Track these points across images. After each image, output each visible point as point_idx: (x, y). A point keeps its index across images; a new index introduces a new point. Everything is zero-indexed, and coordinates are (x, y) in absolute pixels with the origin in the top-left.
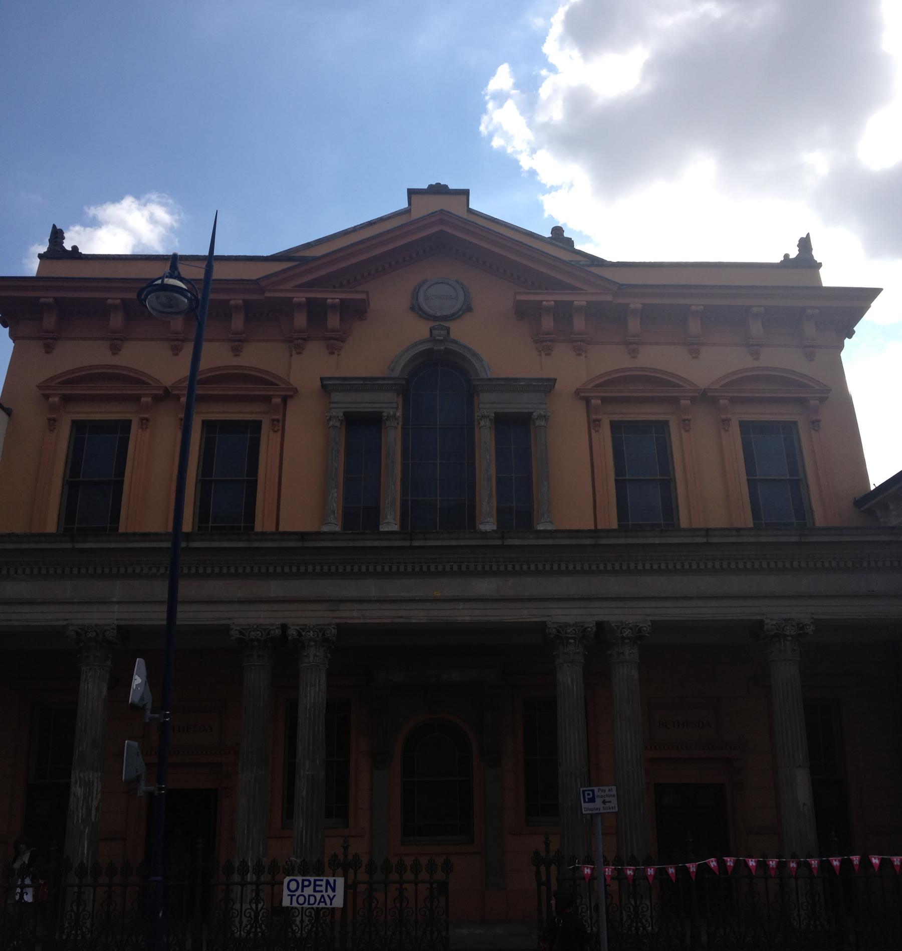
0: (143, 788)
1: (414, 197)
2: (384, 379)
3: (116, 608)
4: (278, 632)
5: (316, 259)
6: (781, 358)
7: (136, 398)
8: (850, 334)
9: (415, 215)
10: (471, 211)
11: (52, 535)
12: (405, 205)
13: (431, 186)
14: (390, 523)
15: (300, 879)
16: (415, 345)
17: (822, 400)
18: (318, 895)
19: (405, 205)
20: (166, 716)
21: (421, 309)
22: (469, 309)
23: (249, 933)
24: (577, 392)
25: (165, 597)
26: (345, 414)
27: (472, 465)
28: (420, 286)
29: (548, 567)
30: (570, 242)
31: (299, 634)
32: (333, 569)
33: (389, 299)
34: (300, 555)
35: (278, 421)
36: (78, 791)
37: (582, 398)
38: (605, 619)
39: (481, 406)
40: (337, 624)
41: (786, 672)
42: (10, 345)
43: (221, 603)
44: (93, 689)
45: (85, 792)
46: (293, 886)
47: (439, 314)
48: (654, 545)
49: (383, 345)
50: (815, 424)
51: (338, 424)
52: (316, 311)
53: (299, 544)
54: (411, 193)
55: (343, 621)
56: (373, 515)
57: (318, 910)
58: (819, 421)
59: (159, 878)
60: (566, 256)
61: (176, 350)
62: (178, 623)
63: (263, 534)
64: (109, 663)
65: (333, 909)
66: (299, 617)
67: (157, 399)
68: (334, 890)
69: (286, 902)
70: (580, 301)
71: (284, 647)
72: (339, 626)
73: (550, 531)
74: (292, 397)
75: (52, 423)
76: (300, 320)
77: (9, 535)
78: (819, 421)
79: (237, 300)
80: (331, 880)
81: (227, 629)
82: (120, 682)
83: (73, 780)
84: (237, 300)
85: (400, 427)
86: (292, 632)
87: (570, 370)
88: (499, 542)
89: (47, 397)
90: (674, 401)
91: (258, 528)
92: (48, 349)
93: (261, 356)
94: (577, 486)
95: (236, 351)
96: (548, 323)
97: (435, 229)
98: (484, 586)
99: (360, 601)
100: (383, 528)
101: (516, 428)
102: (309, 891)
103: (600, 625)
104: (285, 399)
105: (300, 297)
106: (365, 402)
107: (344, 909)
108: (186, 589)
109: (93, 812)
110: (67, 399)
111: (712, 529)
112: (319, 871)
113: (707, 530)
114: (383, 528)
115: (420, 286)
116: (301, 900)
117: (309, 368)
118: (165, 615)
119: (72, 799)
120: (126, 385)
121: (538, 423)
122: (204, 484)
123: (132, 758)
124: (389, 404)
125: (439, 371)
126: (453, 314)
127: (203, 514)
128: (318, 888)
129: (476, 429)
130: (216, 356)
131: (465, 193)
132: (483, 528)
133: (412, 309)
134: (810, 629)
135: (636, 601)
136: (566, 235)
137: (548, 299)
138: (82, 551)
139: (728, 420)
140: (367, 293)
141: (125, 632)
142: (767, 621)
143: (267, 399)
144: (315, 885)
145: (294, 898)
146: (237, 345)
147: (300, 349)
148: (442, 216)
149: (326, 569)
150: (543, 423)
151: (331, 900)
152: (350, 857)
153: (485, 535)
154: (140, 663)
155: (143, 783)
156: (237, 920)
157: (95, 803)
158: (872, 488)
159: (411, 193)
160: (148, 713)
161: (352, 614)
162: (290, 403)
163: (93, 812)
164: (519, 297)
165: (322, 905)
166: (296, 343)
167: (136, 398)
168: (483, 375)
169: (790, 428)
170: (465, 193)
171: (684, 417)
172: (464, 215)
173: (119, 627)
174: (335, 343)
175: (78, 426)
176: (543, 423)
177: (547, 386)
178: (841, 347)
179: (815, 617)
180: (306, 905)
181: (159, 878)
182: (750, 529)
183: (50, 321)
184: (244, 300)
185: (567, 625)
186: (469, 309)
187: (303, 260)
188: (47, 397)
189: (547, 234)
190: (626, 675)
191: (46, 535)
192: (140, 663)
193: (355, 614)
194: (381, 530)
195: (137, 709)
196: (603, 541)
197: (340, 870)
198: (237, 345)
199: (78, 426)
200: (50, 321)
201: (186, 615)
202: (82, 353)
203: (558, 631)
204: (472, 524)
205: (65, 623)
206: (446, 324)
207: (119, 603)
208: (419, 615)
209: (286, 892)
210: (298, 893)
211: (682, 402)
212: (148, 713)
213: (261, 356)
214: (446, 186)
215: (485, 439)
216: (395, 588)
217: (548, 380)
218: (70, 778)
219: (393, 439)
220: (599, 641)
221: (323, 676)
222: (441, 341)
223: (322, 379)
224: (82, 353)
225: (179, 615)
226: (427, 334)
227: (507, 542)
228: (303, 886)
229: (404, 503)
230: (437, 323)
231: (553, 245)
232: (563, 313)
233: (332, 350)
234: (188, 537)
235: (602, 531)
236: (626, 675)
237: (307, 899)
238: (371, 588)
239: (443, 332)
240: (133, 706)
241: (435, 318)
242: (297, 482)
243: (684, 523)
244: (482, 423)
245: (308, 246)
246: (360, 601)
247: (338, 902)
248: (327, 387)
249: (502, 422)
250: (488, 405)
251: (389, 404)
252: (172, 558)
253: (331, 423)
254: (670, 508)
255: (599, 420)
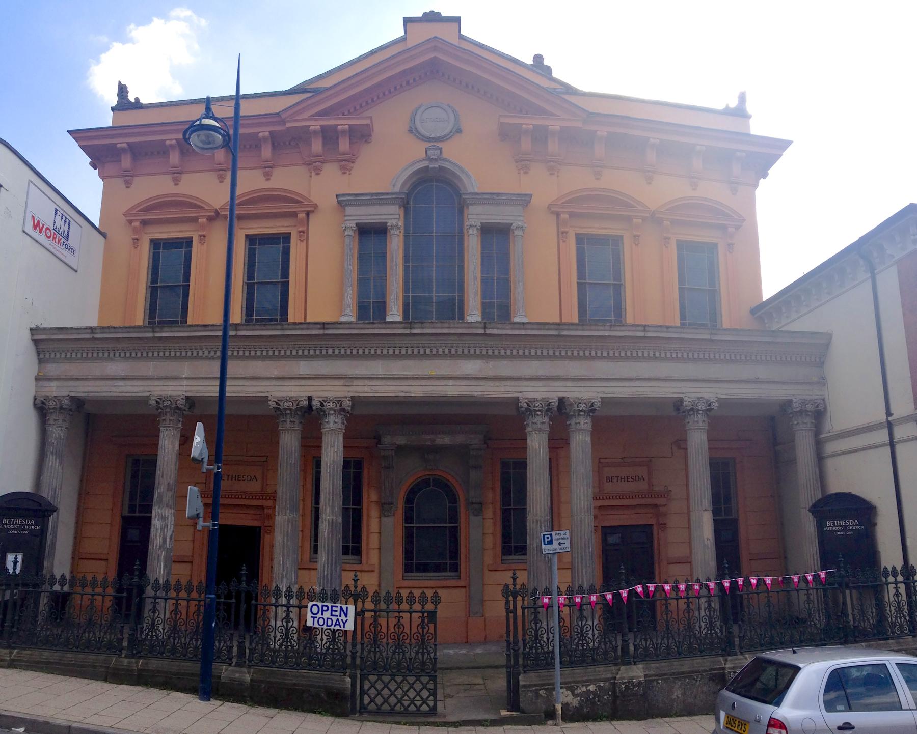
0: (201, 523)
1: (408, 25)
2: (387, 194)
3: (185, 383)
4: (306, 403)
5: (327, 89)
6: (713, 191)
7: (195, 220)
8: (765, 175)
9: (410, 43)
10: (462, 38)
11: (139, 327)
12: (400, 33)
13: (425, 14)
14: (395, 314)
15: (320, 604)
16: (414, 164)
17: (737, 228)
18: (334, 619)
19: (400, 33)
20: (218, 468)
21: (418, 132)
22: (459, 131)
23: (281, 645)
24: (549, 207)
25: (218, 374)
26: (357, 224)
27: (461, 267)
28: (416, 110)
29: (521, 353)
30: (548, 70)
31: (322, 405)
32: (349, 352)
33: (388, 119)
34: (324, 340)
35: (303, 232)
36: (156, 523)
37: (553, 213)
38: (565, 395)
39: (470, 217)
40: (352, 397)
41: (698, 439)
42: (100, 183)
43: (264, 380)
44: (168, 444)
45: (163, 525)
46: (315, 610)
47: (433, 136)
48: (605, 337)
49: (384, 168)
50: (730, 246)
51: (351, 233)
52: (329, 136)
53: (321, 332)
54: (407, 21)
55: (356, 394)
56: (381, 308)
57: (334, 632)
58: (733, 244)
59: (213, 596)
60: (544, 83)
61: (221, 179)
62: (227, 394)
63: (295, 324)
64: (180, 425)
65: (346, 631)
66: (322, 391)
67: (211, 219)
68: (346, 615)
69: (309, 623)
70: (554, 125)
71: (310, 415)
72: (353, 398)
73: (523, 324)
74: (313, 211)
75: (136, 241)
76: (317, 146)
77: (108, 327)
78: (733, 244)
79: (264, 132)
80: (344, 607)
81: (265, 400)
82: (186, 440)
83: (153, 515)
84: (264, 132)
85: (402, 235)
86: (316, 403)
87: (544, 187)
88: (482, 331)
89: (130, 222)
90: (629, 219)
91: (291, 319)
92: (128, 184)
93: (289, 178)
94: (543, 290)
95: (268, 176)
96: (526, 144)
97: (431, 55)
98: (471, 367)
99: (370, 378)
100: (389, 319)
101: (497, 235)
102: (327, 615)
103: (561, 400)
104: (308, 214)
105: (315, 125)
106: (371, 215)
107: (354, 632)
108: (233, 368)
109: (168, 540)
110: (144, 223)
111: (648, 326)
112: (335, 599)
113: (645, 326)
114: (389, 319)
115: (416, 110)
116: (321, 622)
117: (323, 187)
118: (218, 389)
119: (152, 530)
120: (184, 208)
121: (516, 233)
122: (250, 288)
123: (194, 502)
124: (392, 215)
125: (433, 189)
126: (445, 136)
127: (249, 310)
128: (334, 613)
129: (466, 237)
130: (250, 181)
131: (457, 20)
132: (469, 319)
133: (410, 131)
134: (715, 405)
135: (590, 382)
136: (546, 63)
137: (528, 122)
138: (160, 338)
139: (669, 238)
140: (371, 118)
141: (191, 401)
142: (685, 399)
143: (294, 215)
144: (332, 611)
145: (316, 620)
146: (268, 169)
147: (318, 171)
148: (435, 43)
149: (343, 352)
150: (520, 233)
151: (344, 624)
152: (359, 589)
153: (470, 325)
154: (200, 426)
155: (201, 520)
156: (272, 634)
157: (169, 534)
158: (764, 299)
159: (407, 21)
160: (205, 465)
161: (364, 389)
162: (311, 216)
163: (168, 540)
164: (503, 120)
165: (337, 627)
166: (314, 165)
167: (195, 220)
168: (470, 190)
169: (713, 247)
170: (457, 20)
171: (636, 233)
172: (455, 41)
173: (187, 398)
174: (346, 163)
175: (156, 244)
176: (520, 233)
177: (524, 200)
178: (756, 185)
179: (719, 396)
180: (325, 627)
181: (213, 596)
182: (676, 327)
183: (126, 161)
184: (270, 132)
185: (535, 400)
186: (459, 131)
187: (317, 91)
188: (130, 222)
189: (529, 61)
190: (581, 441)
191: (134, 327)
192: (200, 426)
193: (366, 389)
194: (387, 320)
195: (198, 462)
196: (565, 333)
197: (351, 599)
198: (268, 169)
199: (156, 244)
200: (126, 161)
201: (233, 389)
202: (153, 186)
203: (528, 405)
204: (462, 317)
205: (148, 394)
206: (439, 145)
207: (186, 378)
208: (416, 390)
209: (309, 615)
210: (316, 616)
211: (635, 220)
212: (205, 465)
213: (289, 178)
214: (439, 14)
215: (473, 245)
216: (397, 368)
217: (525, 195)
218: (151, 512)
219: (396, 245)
220: (560, 413)
221: (341, 438)
222: (436, 160)
223: (337, 196)
224: (153, 186)
225: (228, 389)
226: (423, 155)
227: (488, 331)
228: (323, 611)
229: (406, 297)
230: (432, 144)
231: (534, 71)
232: (540, 136)
233: (345, 170)
234: (236, 327)
235: (565, 324)
236: (581, 441)
237: (326, 621)
238: (378, 367)
239: (437, 152)
240: (194, 459)
241: (430, 140)
242: (322, 284)
243: (629, 321)
244: (471, 232)
245: (320, 77)
246: (370, 378)
247: (350, 626)
248: (343, 202)
249: (487, 230)
250: (476, 215)
251: (392, 215)
252: (224, 345)
253: (346, 233)
254: (619, 309)
255: (566, 232)
